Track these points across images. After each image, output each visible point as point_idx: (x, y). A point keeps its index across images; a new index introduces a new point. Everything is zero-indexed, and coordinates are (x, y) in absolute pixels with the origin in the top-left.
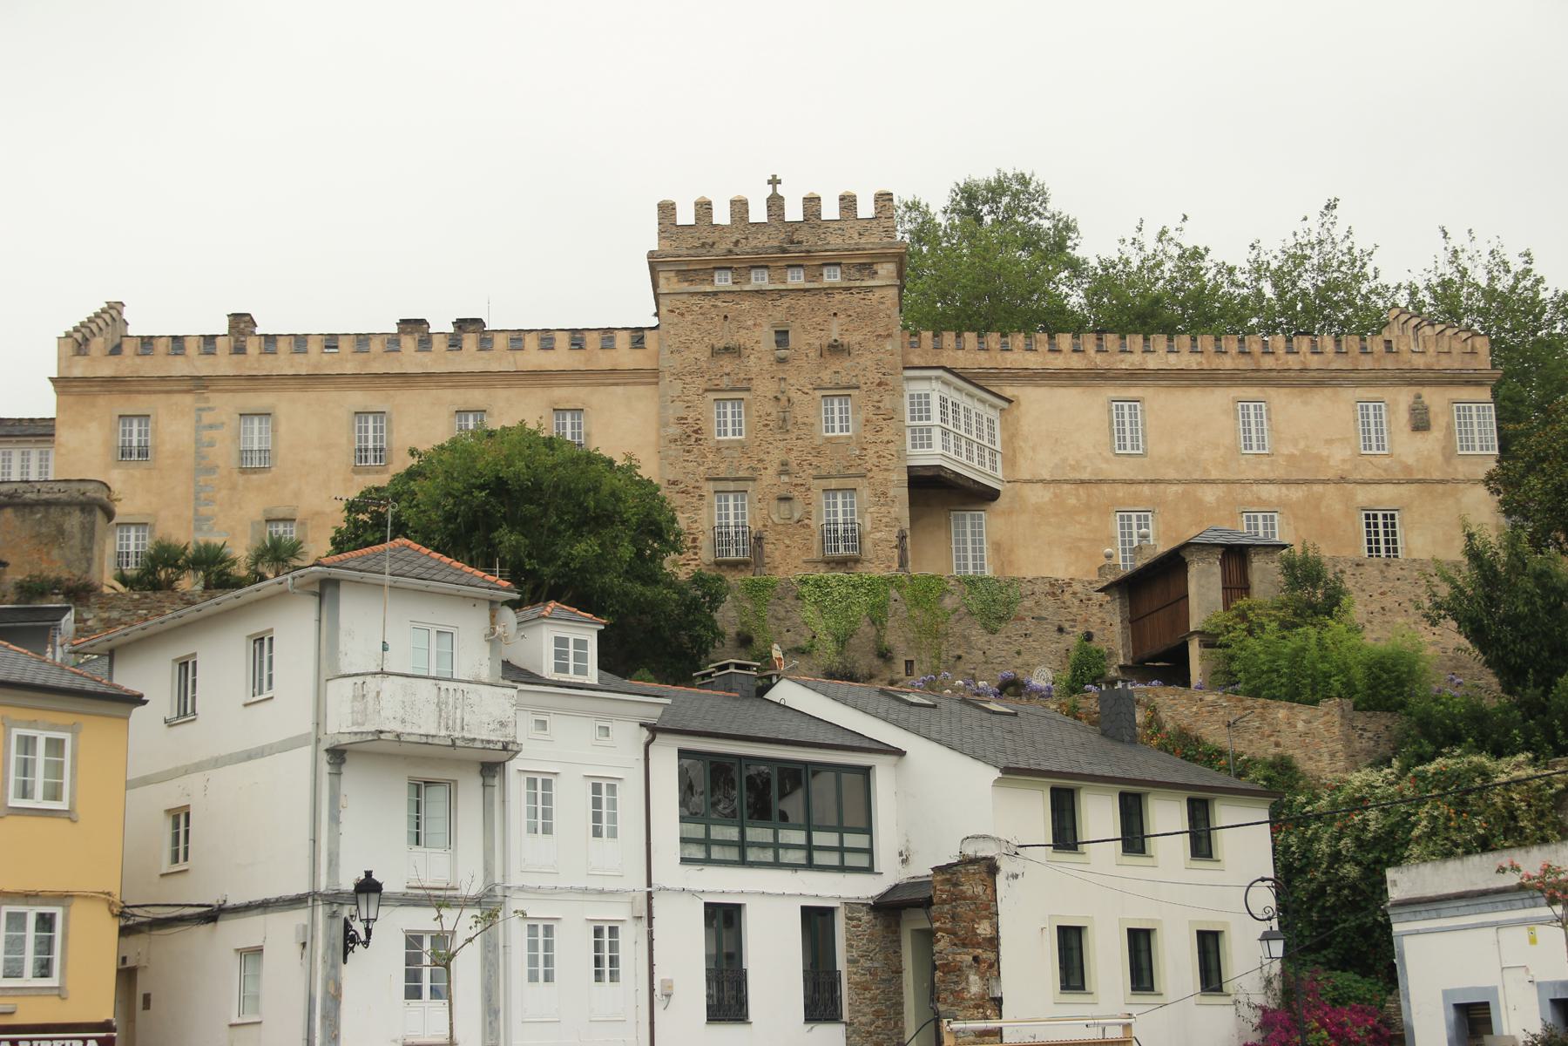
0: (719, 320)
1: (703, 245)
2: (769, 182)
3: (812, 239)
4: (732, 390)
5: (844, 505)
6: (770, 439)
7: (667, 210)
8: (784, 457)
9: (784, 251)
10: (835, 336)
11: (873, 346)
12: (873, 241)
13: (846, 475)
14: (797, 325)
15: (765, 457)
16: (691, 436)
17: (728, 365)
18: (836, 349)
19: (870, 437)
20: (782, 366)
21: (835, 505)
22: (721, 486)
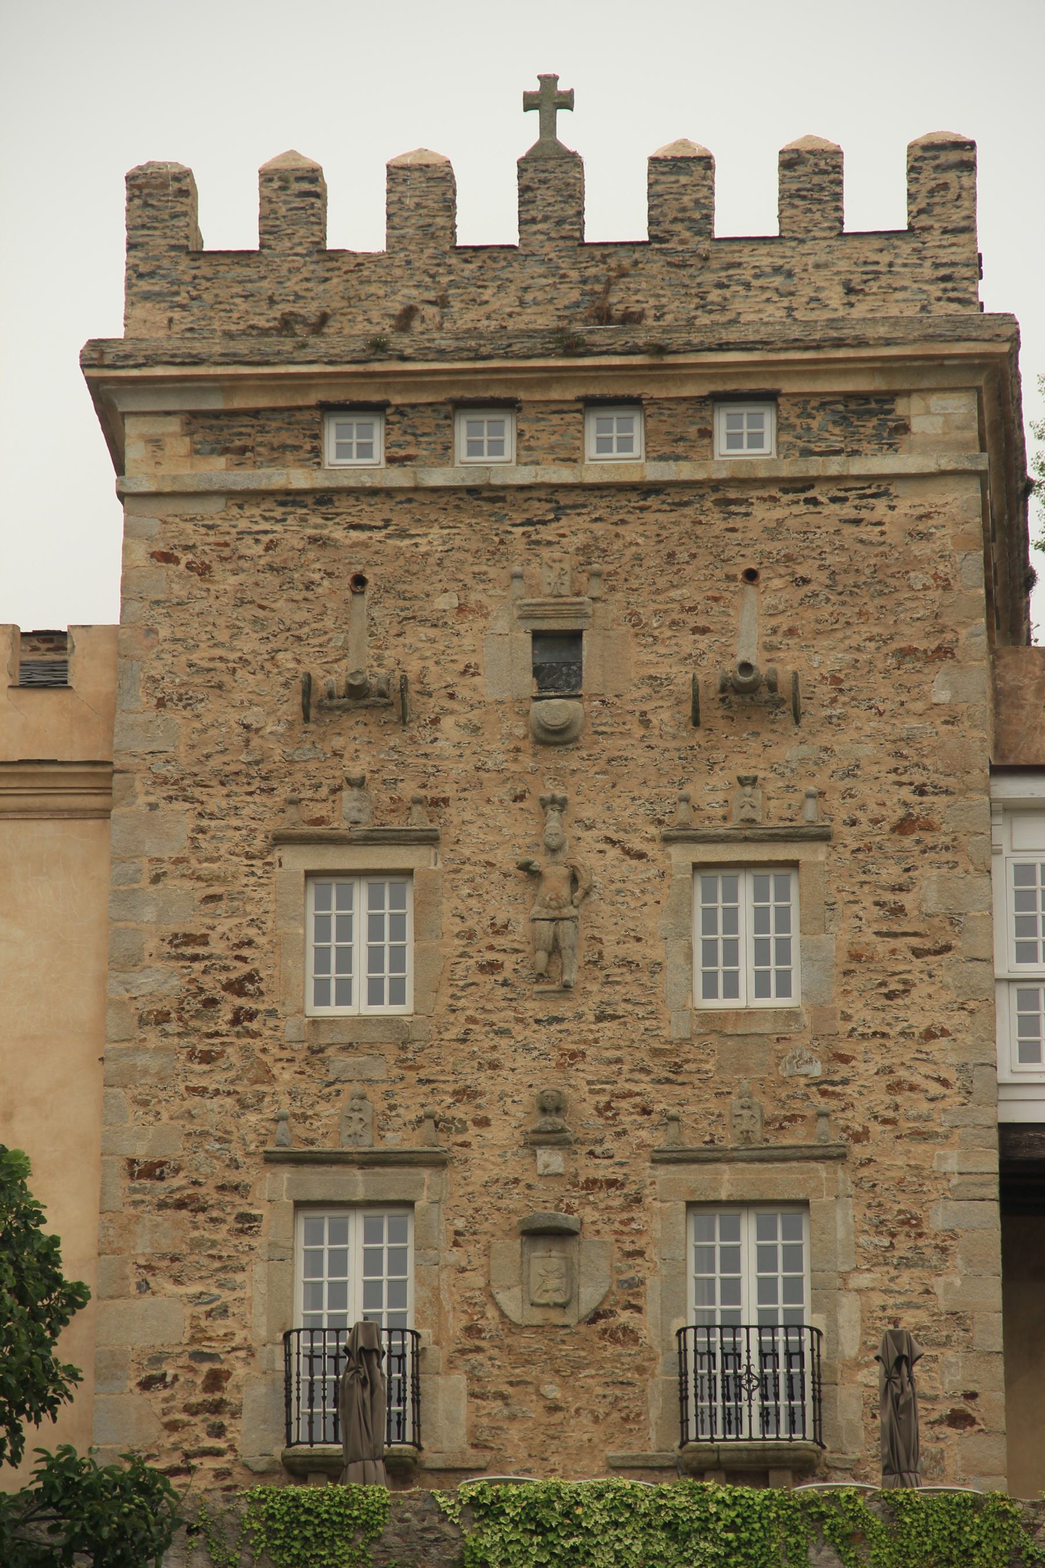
1: (286, 324)
2: (530, 102)
3: (677, 308)
4: (371, 839)
5: (766, 1259)
6: (503, 1017)
7: (159, 198)
8: (552, 1081)
9: (572, 346)
10: (748, 651)
11: (884, 690)
12: (892, 314)
13: (774, 1150)
14: (614, 609)
15: (482, 1080)
16: (216, 1001)
18: (750, 698)
19: (864, 1015)
20: (553, 758)
21: (732, 1259)
22: (319, 1183)
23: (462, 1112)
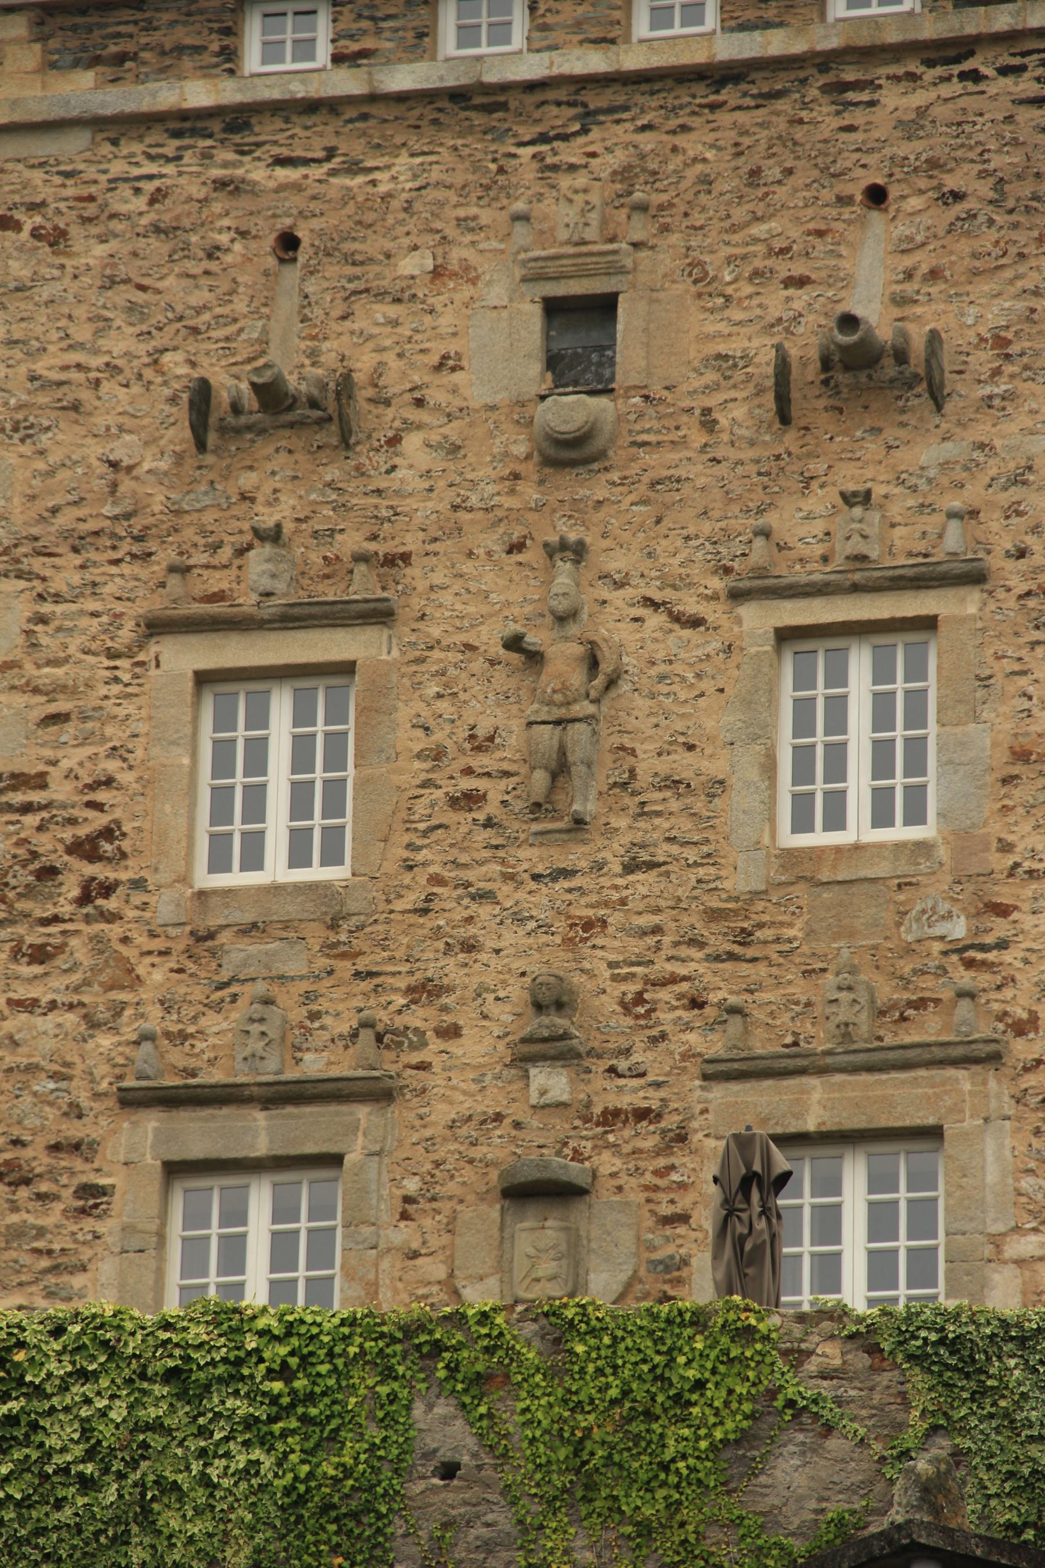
0: (249, 259)
4: (293, 619)
5: (881, 1220)
14: (665, 259)
15: (451, 969)
17: (278, 483)
18: (865, 373)
20: (574, 487)
22: (200, 1134)
23: (419, 1018)
